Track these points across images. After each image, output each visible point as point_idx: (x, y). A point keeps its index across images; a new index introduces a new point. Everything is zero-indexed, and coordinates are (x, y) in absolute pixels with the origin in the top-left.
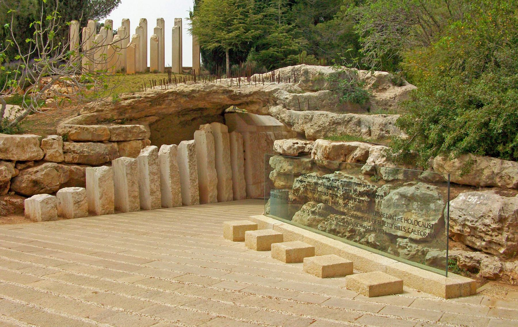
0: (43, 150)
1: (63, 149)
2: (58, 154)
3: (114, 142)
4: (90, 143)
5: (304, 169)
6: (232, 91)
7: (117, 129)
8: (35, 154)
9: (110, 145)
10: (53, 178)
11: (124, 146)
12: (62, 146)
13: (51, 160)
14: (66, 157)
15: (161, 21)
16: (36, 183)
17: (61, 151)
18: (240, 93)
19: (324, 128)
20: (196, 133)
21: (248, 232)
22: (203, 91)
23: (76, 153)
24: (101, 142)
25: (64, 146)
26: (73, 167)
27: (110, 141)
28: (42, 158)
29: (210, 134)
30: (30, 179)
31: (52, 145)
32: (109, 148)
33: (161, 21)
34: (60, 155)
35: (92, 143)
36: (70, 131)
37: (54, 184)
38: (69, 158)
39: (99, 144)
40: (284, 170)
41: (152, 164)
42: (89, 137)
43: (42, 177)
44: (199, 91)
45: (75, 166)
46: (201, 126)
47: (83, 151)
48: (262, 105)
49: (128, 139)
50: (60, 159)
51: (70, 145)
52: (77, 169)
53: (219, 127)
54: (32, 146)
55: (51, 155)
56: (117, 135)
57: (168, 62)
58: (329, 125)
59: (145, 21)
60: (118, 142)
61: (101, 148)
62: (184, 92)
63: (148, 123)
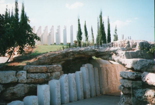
0: (17, 78)
1: (27, 77)
2: (24, 80)
3: (48, 72)
4: (38, 74)
5: (138, 86)
6: (96, 51)
7: (50, 67)
8: (14, 80)
9: (47, 74)
10: (21, 91)
11: (53, 74)
12: (26, 75)
13: (21, 82)
14: (28, 80)
15: (59, 27)
16: (13, 94)
17: (26, 78)
18: (100, 51)
19: (146, 66)
20: (81, 68)
21: (39, 87)
22: (85, 51)
23: (33, 78)
24: (43, 73)
25: (27, 75)
26: (31, 85)
27: (47, 72)
28: (17, 81)
29: (87, 68)
30: (10, 92)
31: (21, 75)
32: (47, 76)
33: (59, 27)
34: (25, 80)
35: (40, 74)
36: (30, 69)
37: (22, 94)
38: (29, 81)
39: (43, 74)
40: (129, 86)
41: (66, 82)
42: (39, 71)
43: (16, 91)
44: (83, 51)
45: (32, 85)
46: (83, 65)
47: (36, 77)
48: (109, 56)
49: (54, 71)
50: (25, 82)
51: (33, 75)
52: (33, 86)
53: (90, 66)
54: (12, 76)
55: (21, 80)
56: (50, 69)
57: (62, 41)
58: (148, 65)
59: (53, 26)
60: (50, 73)
61: (44, 76)
62: (76, 51)
63: (61, 64)
